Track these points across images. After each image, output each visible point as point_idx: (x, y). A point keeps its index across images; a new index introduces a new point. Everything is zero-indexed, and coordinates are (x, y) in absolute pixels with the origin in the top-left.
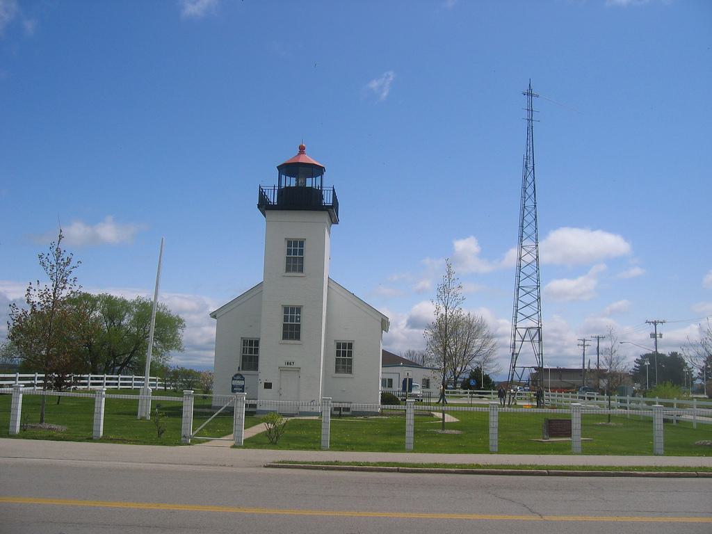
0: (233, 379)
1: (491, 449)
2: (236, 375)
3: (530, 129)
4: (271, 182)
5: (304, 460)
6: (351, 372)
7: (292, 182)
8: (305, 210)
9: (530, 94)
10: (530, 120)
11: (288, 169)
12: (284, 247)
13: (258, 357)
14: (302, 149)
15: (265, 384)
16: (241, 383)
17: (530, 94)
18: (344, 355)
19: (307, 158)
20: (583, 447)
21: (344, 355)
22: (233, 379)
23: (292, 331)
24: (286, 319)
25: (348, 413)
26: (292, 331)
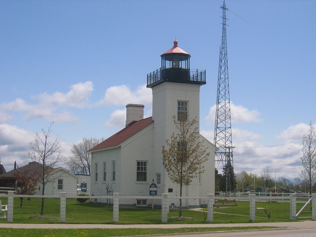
0: (150, 187)
1: (9, 220)
2: (152, 185)
3: (224, 29)
4: (156, 65)
5: (194, 235)
7: (169, 65)
8: (184, 83)
9: (224, 8)
10: (224, 24)
11: (167, 57)
12: (177, 104)
13: (146, 172)
15: (169, 189)
16: (155, 189)
17: (224, 8)
19: (179, 50)
20: (14, 219)
22: (150, 187)
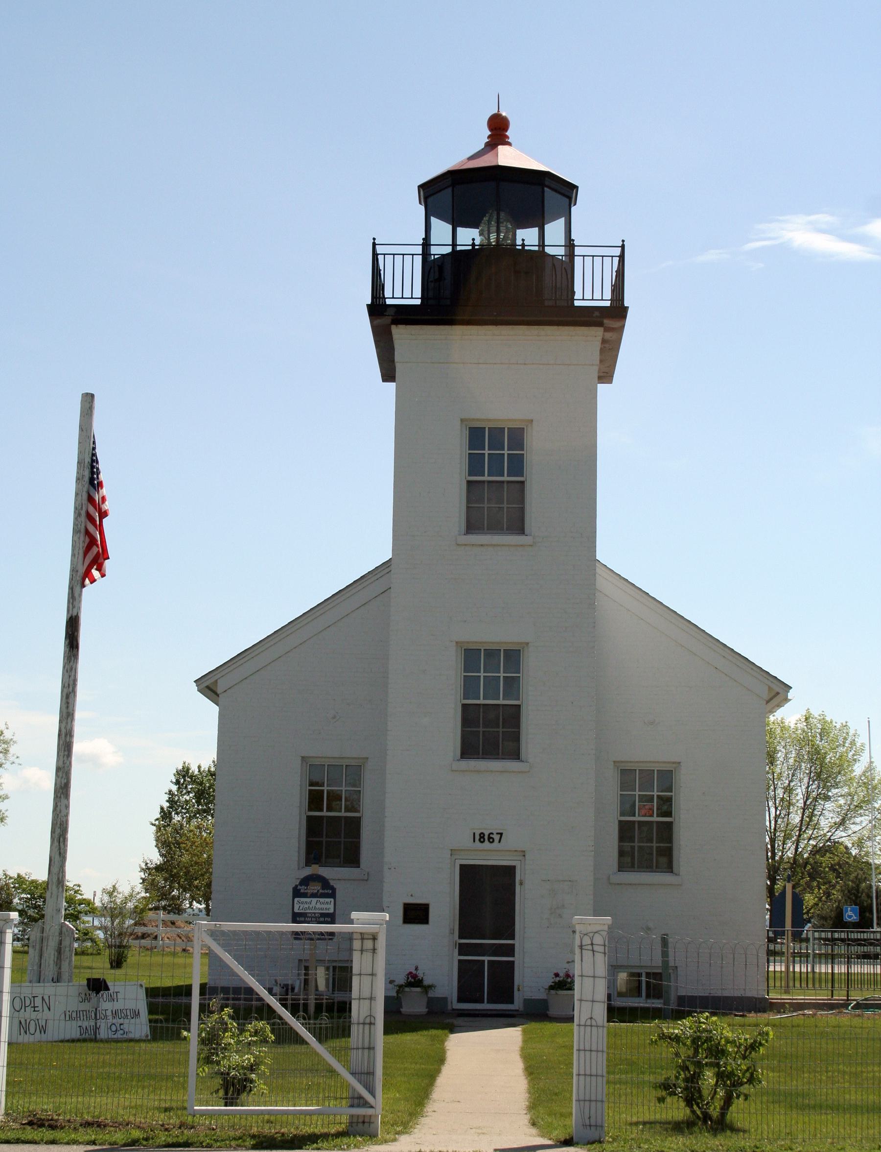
0: (297, 893)
2: (306, 881)
6: (669, 868)
11: (455, 193)
14: (498, 129)
18: (647, 838)
21: (647, 838)
22: (297, 893)
23: (490, 732)
24: (469, 686)
25: (657, 1004)
26: (490, 732)
